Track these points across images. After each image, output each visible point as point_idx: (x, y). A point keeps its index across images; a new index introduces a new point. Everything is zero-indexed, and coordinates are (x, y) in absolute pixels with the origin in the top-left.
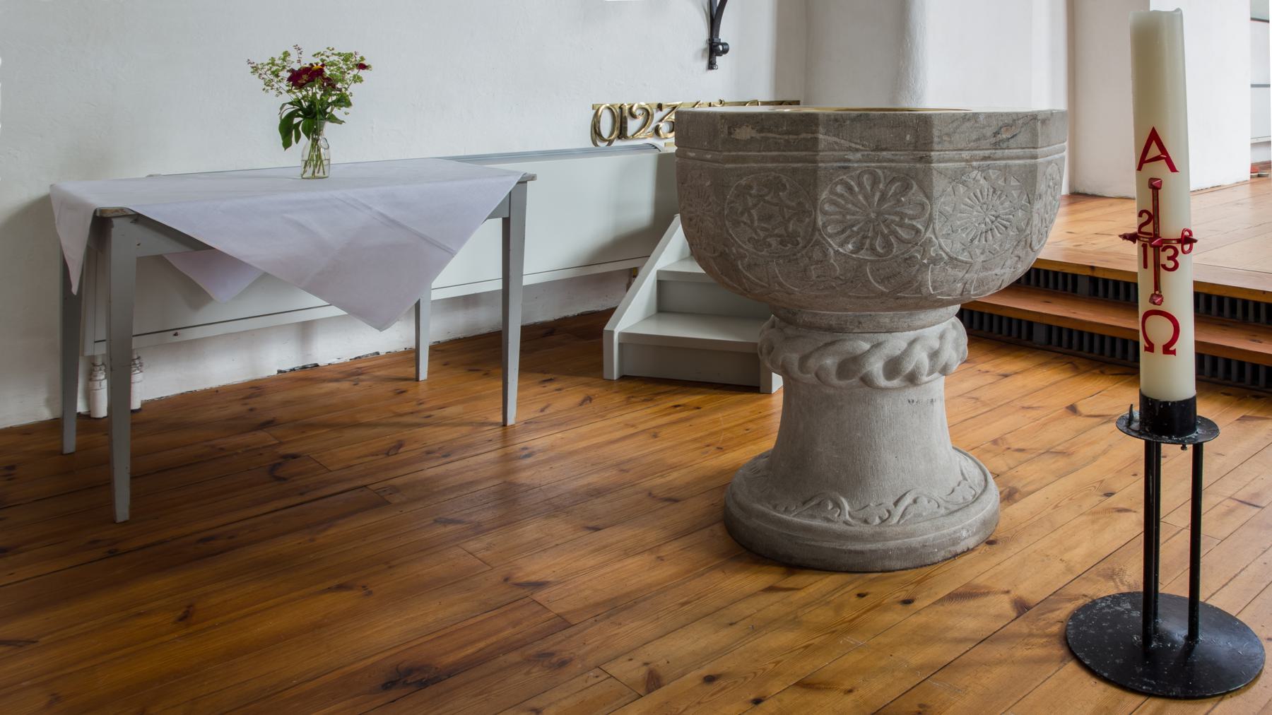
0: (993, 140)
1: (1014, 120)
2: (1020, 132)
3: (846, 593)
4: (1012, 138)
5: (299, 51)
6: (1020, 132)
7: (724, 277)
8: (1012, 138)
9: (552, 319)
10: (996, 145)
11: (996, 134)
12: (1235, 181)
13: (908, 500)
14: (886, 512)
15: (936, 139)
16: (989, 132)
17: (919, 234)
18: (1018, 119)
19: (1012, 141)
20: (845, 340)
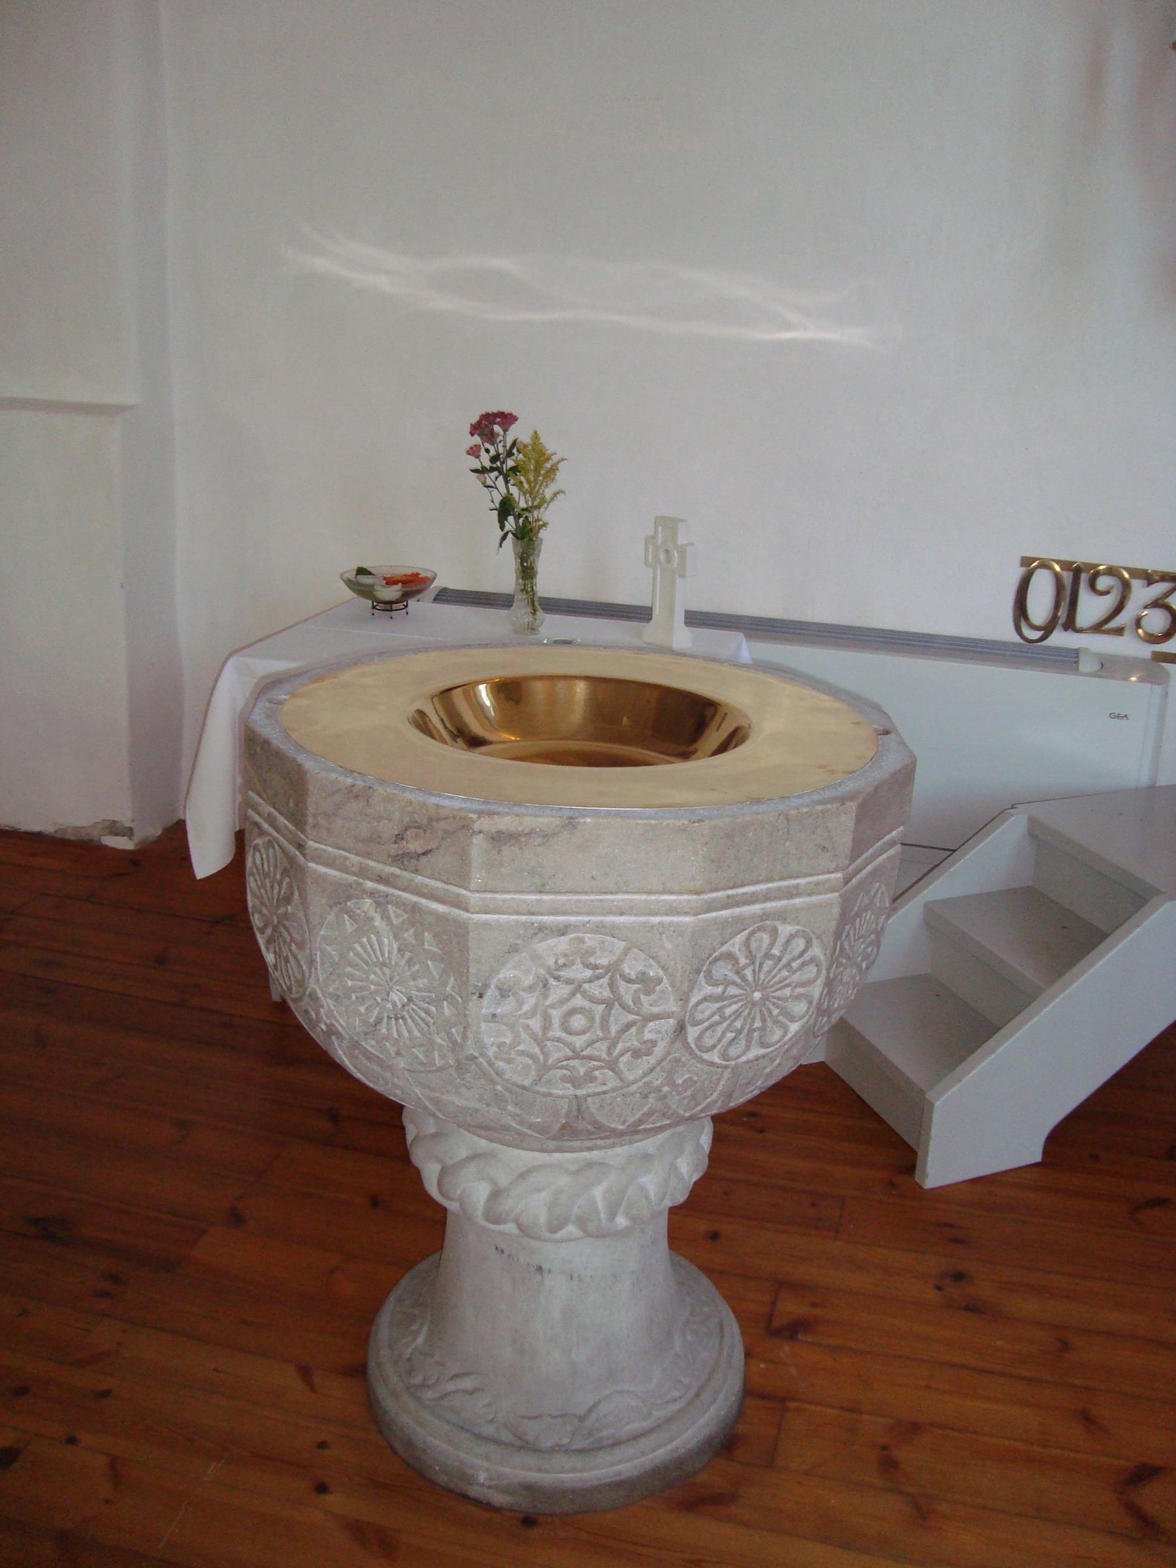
0: (393, 849)
1: (431, 820)
2: (438, 848)
3: (649, 893)
4: (424, 854)
5: (692, 821)
6: (438, 848)
7: (657, 822)
8: (424, 854)
9: (215, 872)
10: (399, 859)
11: (400, 837)
12: (405, 573)
13: (467, 1383)
14: (436, 1377)
15: (310, 820)
16: (388, 829)
17: (314, 963)
18: (438, 820)
19: (423, 859)
20: (1082, 563)
